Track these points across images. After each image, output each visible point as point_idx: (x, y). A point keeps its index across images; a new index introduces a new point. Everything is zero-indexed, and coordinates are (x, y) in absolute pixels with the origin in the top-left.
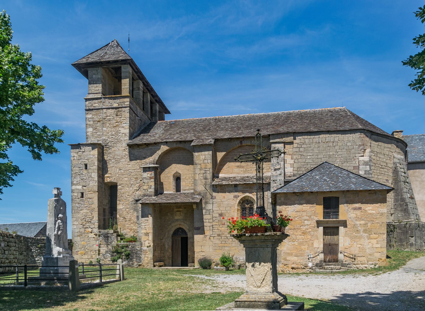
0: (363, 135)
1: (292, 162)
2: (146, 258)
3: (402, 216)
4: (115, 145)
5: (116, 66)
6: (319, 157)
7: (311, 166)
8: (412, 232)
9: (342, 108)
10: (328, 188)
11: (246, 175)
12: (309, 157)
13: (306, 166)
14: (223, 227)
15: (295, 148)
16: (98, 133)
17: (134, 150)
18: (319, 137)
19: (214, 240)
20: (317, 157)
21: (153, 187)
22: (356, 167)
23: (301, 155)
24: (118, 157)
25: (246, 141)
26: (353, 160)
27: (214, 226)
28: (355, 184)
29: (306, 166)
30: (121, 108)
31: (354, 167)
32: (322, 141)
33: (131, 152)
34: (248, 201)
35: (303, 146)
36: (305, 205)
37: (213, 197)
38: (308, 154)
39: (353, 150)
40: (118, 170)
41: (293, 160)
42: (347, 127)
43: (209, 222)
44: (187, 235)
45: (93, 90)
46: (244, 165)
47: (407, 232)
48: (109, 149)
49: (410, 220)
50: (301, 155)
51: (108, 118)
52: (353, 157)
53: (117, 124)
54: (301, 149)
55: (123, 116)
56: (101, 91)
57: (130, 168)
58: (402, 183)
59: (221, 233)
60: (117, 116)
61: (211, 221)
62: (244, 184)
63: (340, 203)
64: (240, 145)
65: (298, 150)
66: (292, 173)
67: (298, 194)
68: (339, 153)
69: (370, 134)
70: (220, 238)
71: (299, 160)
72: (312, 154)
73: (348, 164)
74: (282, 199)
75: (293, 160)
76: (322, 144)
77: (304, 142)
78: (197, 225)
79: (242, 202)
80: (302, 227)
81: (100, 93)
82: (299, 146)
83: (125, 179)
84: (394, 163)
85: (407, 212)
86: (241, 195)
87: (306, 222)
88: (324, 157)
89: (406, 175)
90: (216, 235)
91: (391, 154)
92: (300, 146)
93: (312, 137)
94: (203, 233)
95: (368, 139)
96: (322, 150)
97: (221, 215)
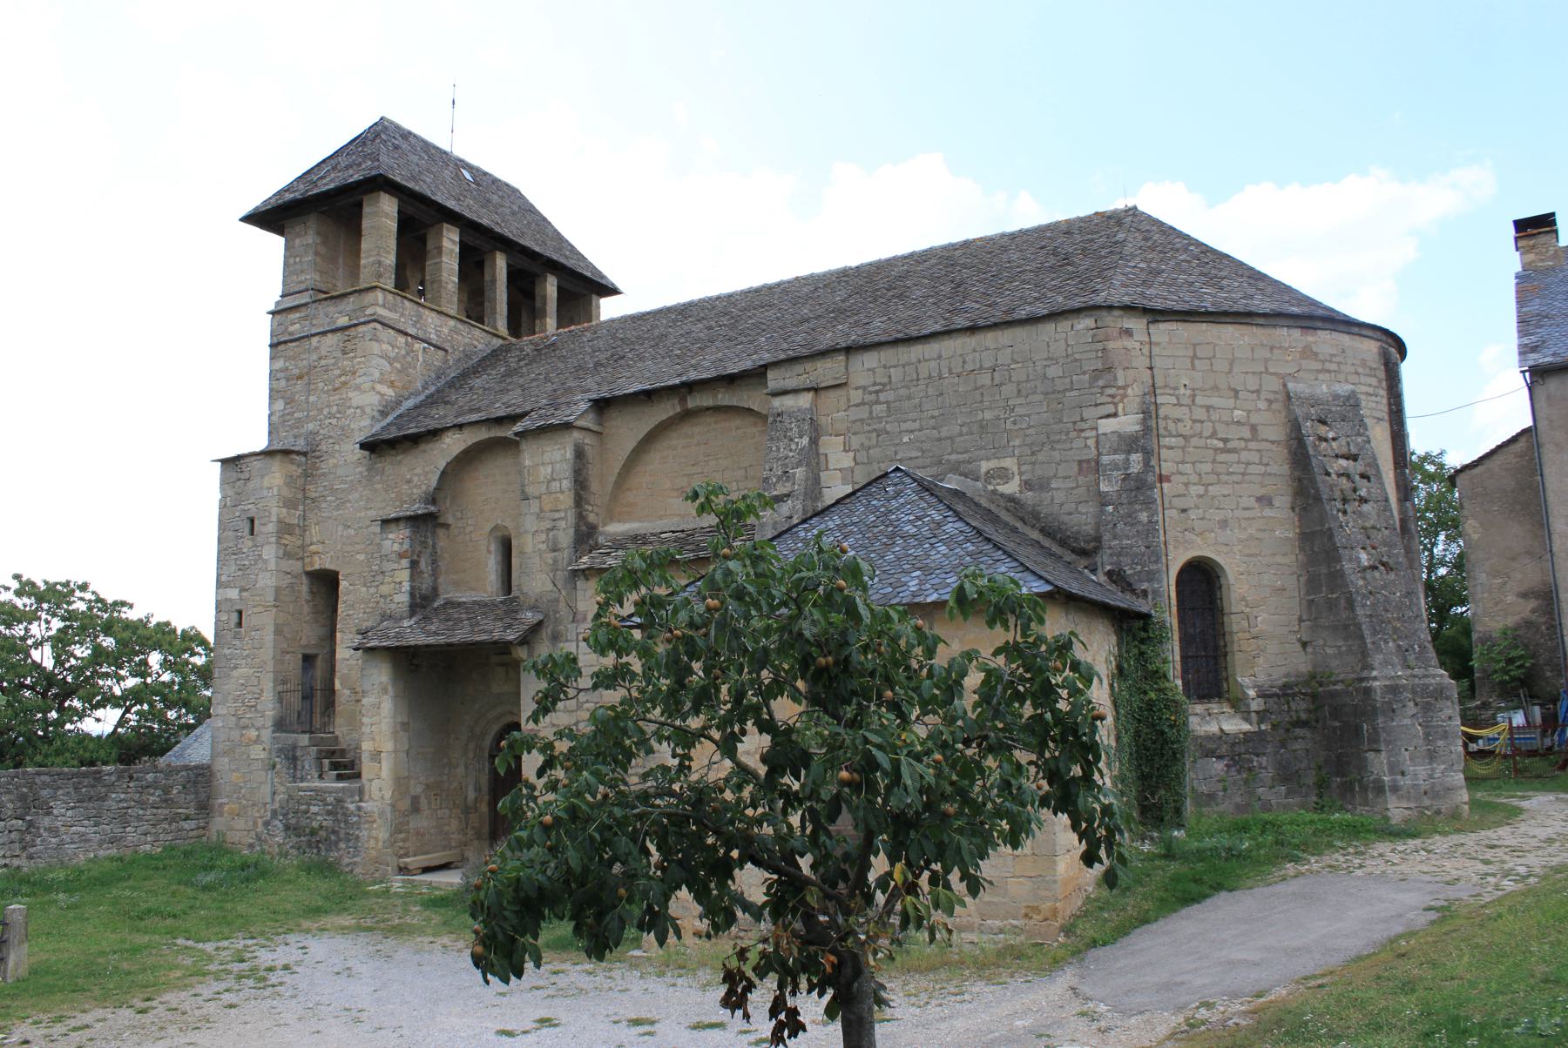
2: (372, 842)
3: (1340, 654)
12: (906, 439)
15: (857, 405)
21: (406, 587)
22: (1088, 461)
31: (1080, 462)
32: (950, 370)
37: (579, 617)
38: (904, 426)
39: (1072, 394)
41: (851, 454)
51: (323, 362)
52: (1075, 423)
53: (343, 379)
54: (879, 409)
55: (359, 353)
65: (865, 415)
68: (1019, 411)
69: (1145, 321)
71: (871, 451)
72: (917, 425)
73: (1056, 454)
76: (952, 380)
77: (886, 380)
82: (868, 398)
88: (961, 434)
92: (873, 397)
96: (955, 403)
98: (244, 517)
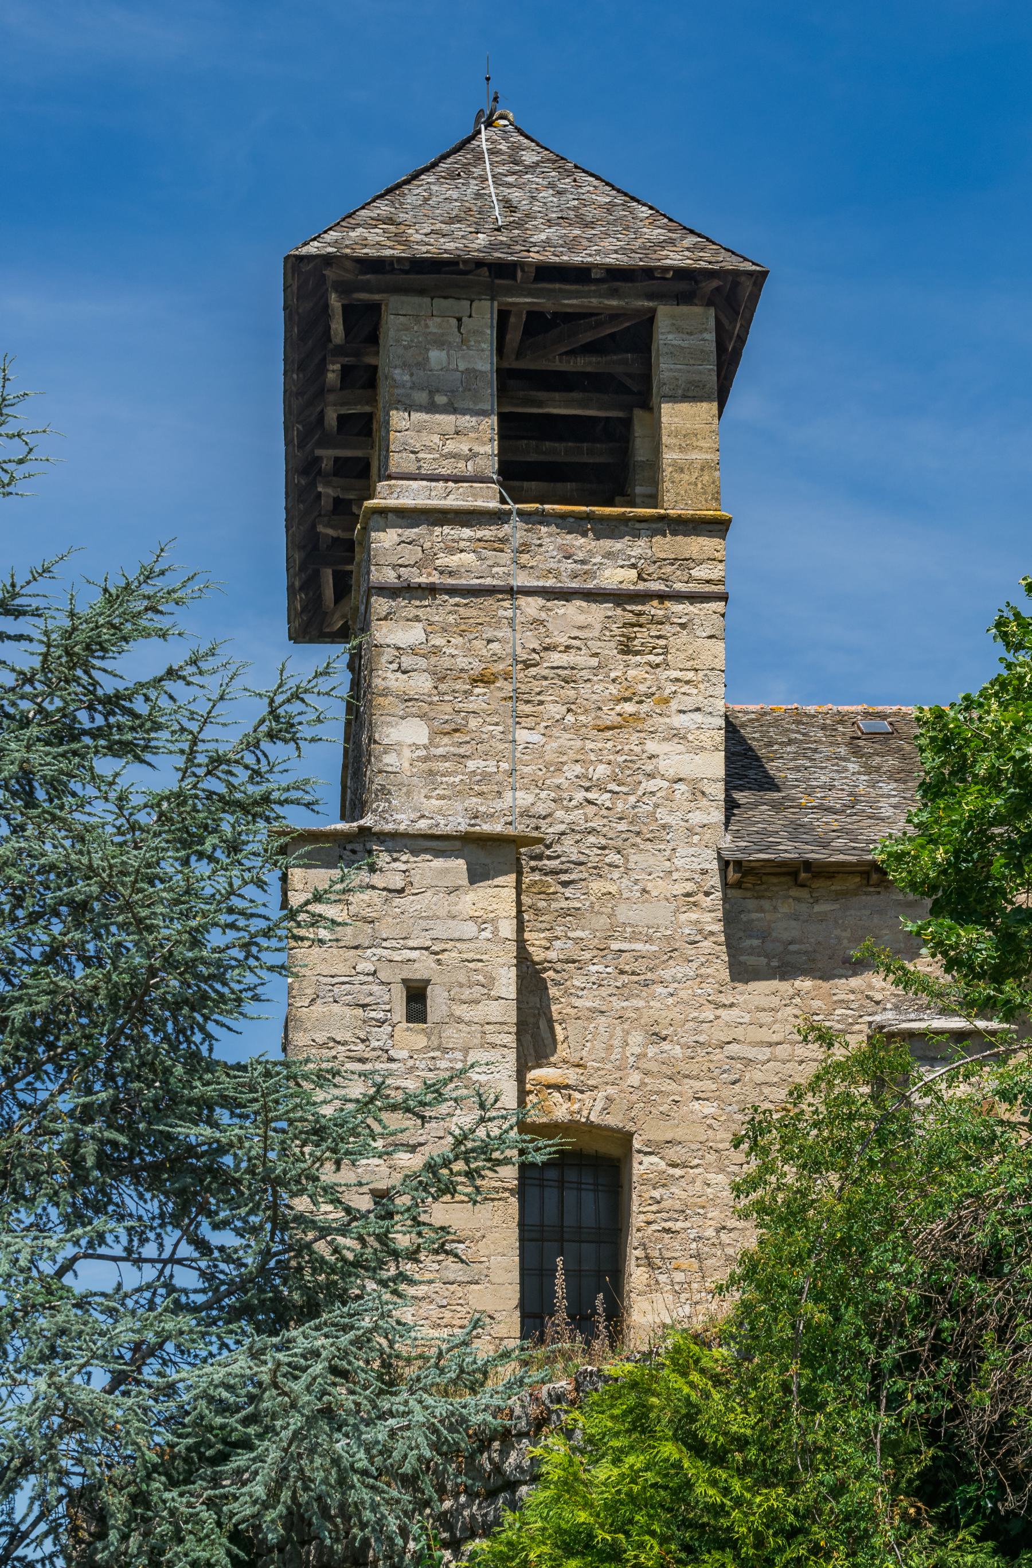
4: (613, 857)
16: (471, 765)
17: (766, 904)
24: (638, 946)
30: (661, 597)
33: (744, 917)
40: (636, 1038)
45: (430, 450)
48: (565, 884)
56: (490, 466)
57: (739, 1033)
60: (626, 649)
83: (696, 1105)
98: (394, 975)
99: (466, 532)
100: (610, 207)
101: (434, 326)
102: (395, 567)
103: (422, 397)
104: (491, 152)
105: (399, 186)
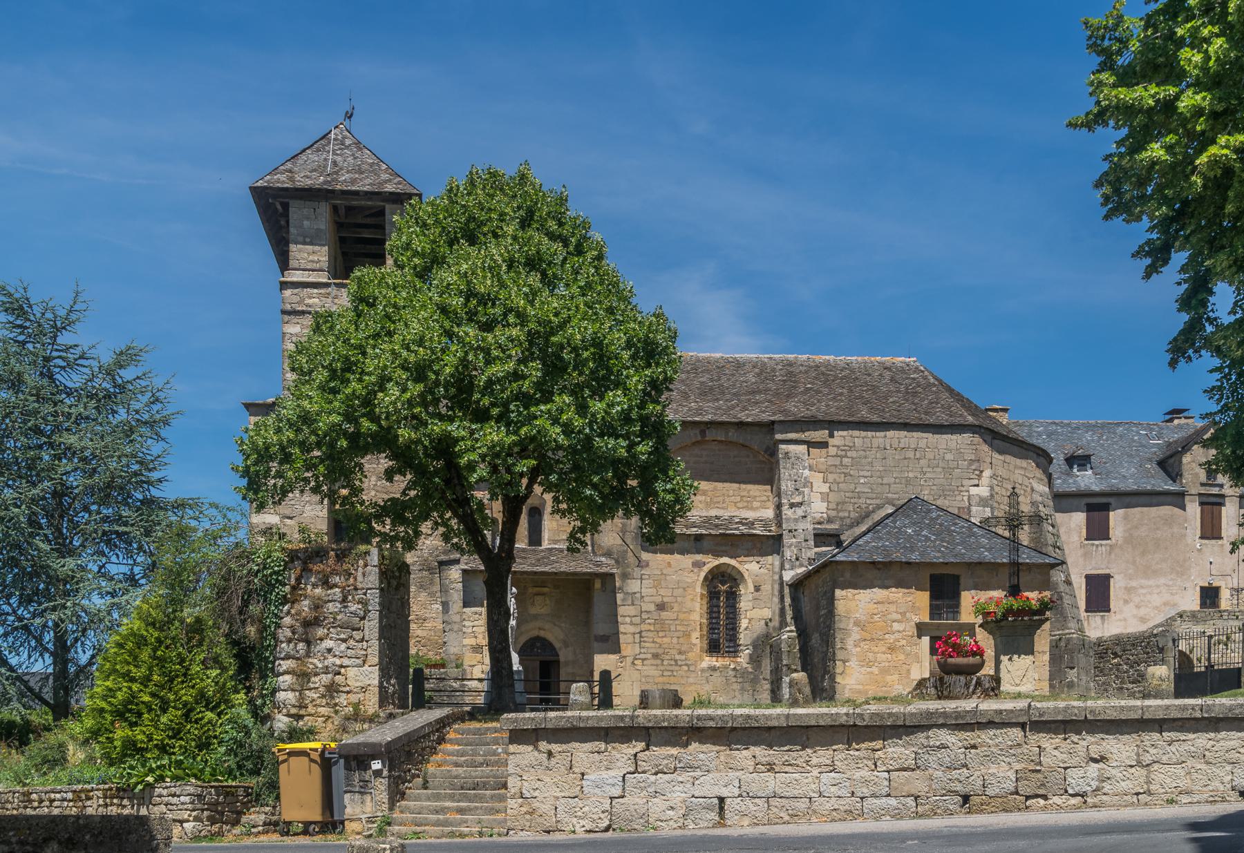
0: (977, 439)
1: (825, 488)
5: (370, 203)
6: (884, 482)
7: (868, 502)
8: (1072, 657)
9: (907, 360)
10: (939, 555)
11: (713, 513)
12: (862, 481)
13: (856, 500)
14: (665, 636)
18: (885, 436)
19: (645, 668)
20: (880, 481)
23: (846, 474)
25: (714, 431)
26: (956, 493)
27: (643, 634)
28: (989, 550)
29: (856, 500)
34: (723, 576)
35: (849, 454)
36: (893, 589)
38: (862, 473)
41: (828, 485)
42: (944, 419)
43: (632, 624)
44: (558, 655)
45: (304, 259)
46: (706, 488)
47: (1061, 657)
49: (1067, 631)
50: (846, 474)
54: (845, 460)
56: (325, 265)
58: (1051, 548)
59: (660, 651)
61: (637, 620)
62: (721, 534)
63: (962, 587)
64: (699, 438)
65: (838, 463)
66: (825, 515)
67: (880, 566)
68: (928, 475)
70: (659, 662)
74: (848, 575)
75: (828, 485)
78: (600, 628)
79: (710, 577)
80: (887, 636)
81: (324, 271)
82: (840, 453)
84: (1033, 503)
85: (1062, 614)
86: (712, 562)
87: (896, 626)
88: (895, 483)
89: (1055, 531)
90: (649, 656)
91: (1026, 482)
92: (843, 453)
93: (870, 434)
94: (616, 649)
95: (986, 448)
97: (661, 607)
99: (316, 291)
100: (372, 165)
101: (305, 211)
102: (290, 304)
103: (300, 239)
104: (335, 139)
105: (297, 155)
